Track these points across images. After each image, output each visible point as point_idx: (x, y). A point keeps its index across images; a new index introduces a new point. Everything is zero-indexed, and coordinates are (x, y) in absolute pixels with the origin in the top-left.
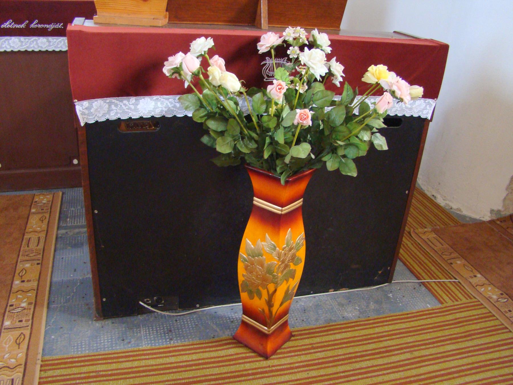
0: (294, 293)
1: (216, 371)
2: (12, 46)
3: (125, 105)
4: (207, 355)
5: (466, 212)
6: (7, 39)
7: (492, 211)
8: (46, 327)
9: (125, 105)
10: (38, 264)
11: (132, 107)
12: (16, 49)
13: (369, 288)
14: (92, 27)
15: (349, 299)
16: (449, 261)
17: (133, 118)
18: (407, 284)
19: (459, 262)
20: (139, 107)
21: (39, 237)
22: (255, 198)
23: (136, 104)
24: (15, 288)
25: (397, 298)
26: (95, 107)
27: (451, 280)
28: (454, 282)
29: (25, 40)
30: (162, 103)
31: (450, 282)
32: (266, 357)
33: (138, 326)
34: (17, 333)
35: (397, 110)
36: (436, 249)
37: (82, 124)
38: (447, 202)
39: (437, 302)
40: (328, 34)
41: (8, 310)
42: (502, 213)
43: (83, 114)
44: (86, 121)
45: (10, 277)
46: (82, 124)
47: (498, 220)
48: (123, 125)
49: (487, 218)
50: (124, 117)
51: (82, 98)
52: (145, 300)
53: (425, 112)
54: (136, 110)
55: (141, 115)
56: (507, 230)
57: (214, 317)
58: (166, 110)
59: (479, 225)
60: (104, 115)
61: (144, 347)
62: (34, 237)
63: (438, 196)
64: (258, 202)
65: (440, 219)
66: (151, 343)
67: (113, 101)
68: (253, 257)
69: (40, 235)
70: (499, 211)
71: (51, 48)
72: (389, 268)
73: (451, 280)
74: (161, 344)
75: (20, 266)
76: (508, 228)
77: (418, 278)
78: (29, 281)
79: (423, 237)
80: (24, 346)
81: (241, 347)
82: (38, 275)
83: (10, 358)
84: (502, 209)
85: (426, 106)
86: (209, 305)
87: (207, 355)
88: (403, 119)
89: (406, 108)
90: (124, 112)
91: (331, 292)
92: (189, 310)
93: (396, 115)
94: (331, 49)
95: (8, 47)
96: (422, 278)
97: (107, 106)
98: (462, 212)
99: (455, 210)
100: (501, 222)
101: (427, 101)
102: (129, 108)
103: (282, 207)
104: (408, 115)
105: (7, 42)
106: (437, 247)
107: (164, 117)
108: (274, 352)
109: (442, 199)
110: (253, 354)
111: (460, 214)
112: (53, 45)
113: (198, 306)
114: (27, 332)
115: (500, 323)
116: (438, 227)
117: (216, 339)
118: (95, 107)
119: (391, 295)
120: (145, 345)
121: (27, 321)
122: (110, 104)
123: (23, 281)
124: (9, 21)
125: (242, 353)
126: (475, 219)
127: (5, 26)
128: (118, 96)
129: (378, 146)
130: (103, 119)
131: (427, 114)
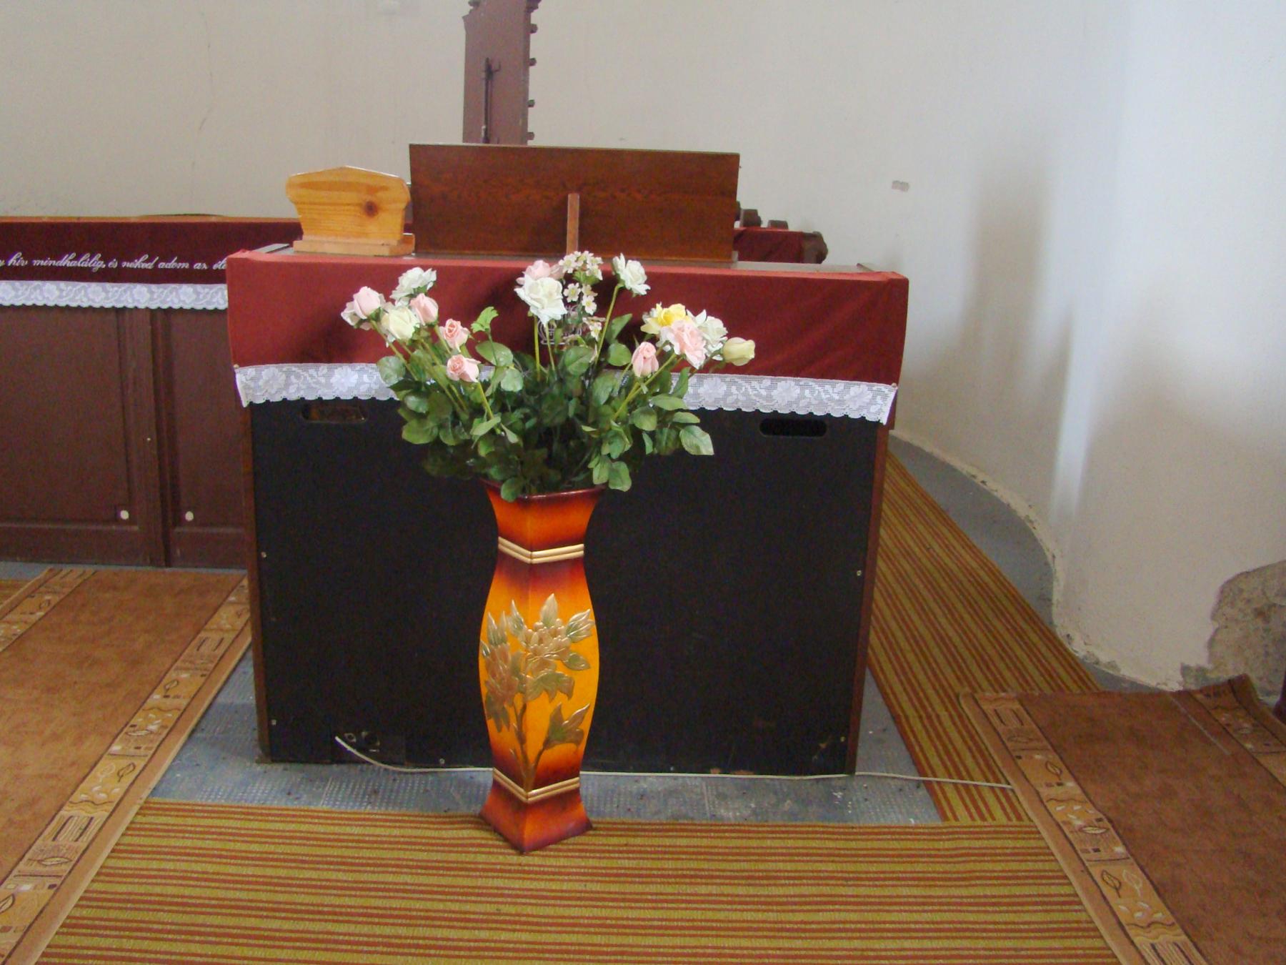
0: (582, 733)
1: (424, 856)
3: (311, 376)
4: (419, 833)
5: (1128, 671)
7: (1185, 670)
8: (174, 760)
9: (311, 376)
10: (202, 676)
11: (323, 380)
13: (797, 778)
15: (745, 791)
16: (1017, 754)
17: (324, 398)
18: (889, 781)
19: (1038, 757)
20: (333, 380)
21: (222, 639)
22: (500, 539)
23: (329, 376)
24: (150, 703)
25: (851, 800)
26: (265, 378)
27: (994, 785)
28: (1003, 790)
30: (370, 376)
31: (992, 788)
32: (520, 848)
33: (324, 780)
34: (124, 763)
35: (810, 403)
36: (1000, 728)
37: (245, 404)
38: (1092, 649)
39: (933, 811)
40: (643, 261)
41: (125, 730)
42: (1208, 675)
43: (246, 387)
44: (250, 399)
45: (148, 688)
46: (245, 404)
47: (1201, 691)
48: (314, 413)
49: (1174, 684)
50: (311, 397)
51: (244, 363)
52: (346, 735)
53: (873, 409)
54: (329, 385)
55: (337, 394)
56: (1213, 712)
57: (463, 783)
58: (377, 387)
59: (1149, 699)
60: (279, 391)
61: (320, 807)
62: (216, 637)
63: (1077, 638)
64: (507, 546)
65: (1049, 674)
66: (334, 805)
67: (294, 369)
68: (496, 645)
69: (226, 635)
70: (1201, 670)
72: (843, 739)
73: (994, 785)
74: (351, 808)
75: (173, 674)
76: (1216, 708)
77: (922, 772)
78: (177, 697)
79: (984, 707)
80: (128, 780)
81: (487, 830)
82: (195, 691)
83: (99, 792)
84: (1209, 666)
85: (874, 398)
86: (464, 764)
87: (419, 833)
88: (827, 423)
89: (830, 399)
90: (309, 387)
91: (715, 775)
92: (421, 767)
93: (811, 414)
96: (929, 772)
97: (284, 377)
98: (1119, 670)
99: (1105, 666)
100: (1208, 696)
101: (875, 388)
102: (318, 383)
103: (532, 550)
104: (837, 414)
105: (83, 292)
107: (373, 399)
108: (541, 845)
109: (1082, 642)
110: (501, 843)
111: (1112, 675)
113: (442, 761)
114: (140, 764)
115: (1057, 868)
116: (1037, 693)
117: (450, 813)
118: (265, 378)
119: (839, 795)
120: (322, 806)
121: (147, 748)
122: (288, 374)
123: (166, 697)
125: (482, 838)
126: (1141, 686)
128: (301, 361)
129: (691, 447)
130: (278, 398)
131: (880, 412)
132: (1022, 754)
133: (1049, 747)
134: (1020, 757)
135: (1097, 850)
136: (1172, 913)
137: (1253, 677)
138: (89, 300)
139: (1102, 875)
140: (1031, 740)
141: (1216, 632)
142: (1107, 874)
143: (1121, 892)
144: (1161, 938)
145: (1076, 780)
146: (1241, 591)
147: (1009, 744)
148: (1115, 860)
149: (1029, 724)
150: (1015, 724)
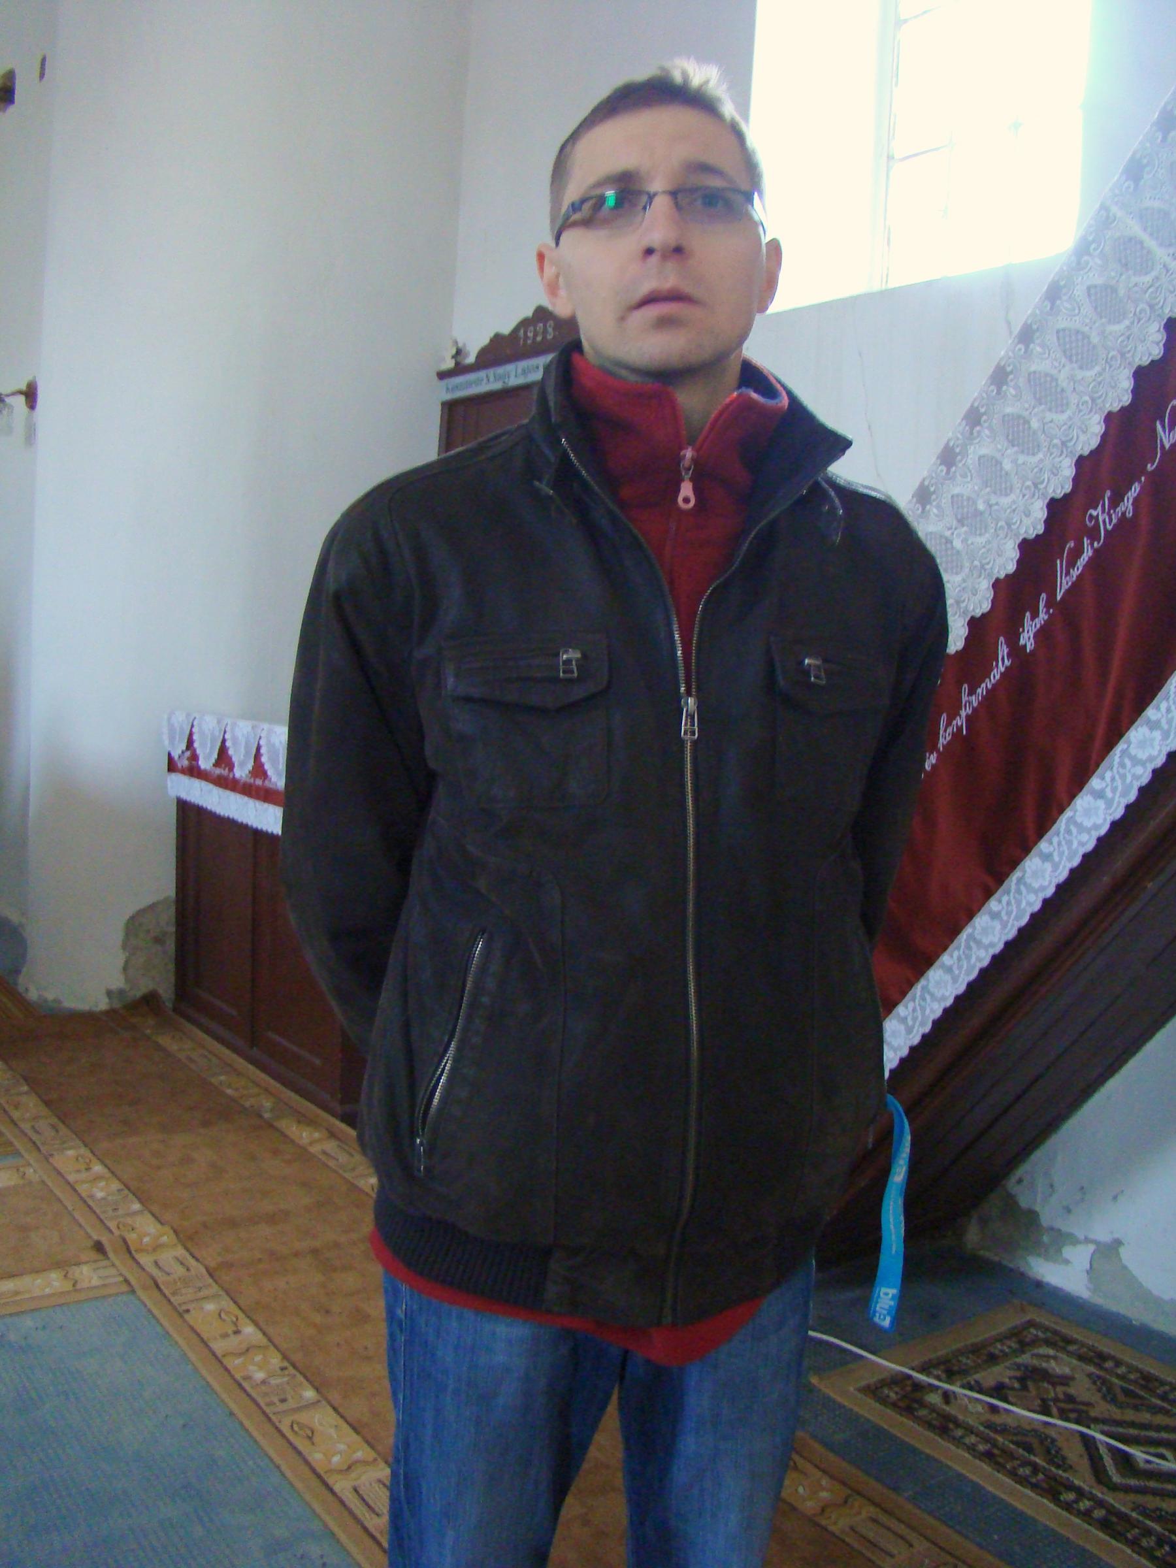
2: (1144, 758)
6: (1123, 752)
7: (109, 993)
12: (1102, 825)
14: (626, 1429)
16: (184, 1307)
29: (1158, 708)
49: (103, 1004)
70: (121, 992)
71: (1011, 929)
84: (127, 988)
94: (844, 470)
95: (1139, 770)
106: (626, 1352)
112: (960, 973)
124: (1026, 620)
127: (1065, 587)
132: (190, 1306)
133: (221, 1293)
134: (188, 1311)
135: (283, 1401)
136: (372, 1447)
137: (161, 991)
138: (1143, 763)
139: (292, 1426)
140: (200, 1289)
141: (127, 962)
142: (298, 1423)
143: (316, 1439)
144: (364, 1478)
145: (256, 1324)
146: (140, 925)
147: (172, 1299)
148: (135, 1213)
149: (197, 1268)
150: (180, 1271)
